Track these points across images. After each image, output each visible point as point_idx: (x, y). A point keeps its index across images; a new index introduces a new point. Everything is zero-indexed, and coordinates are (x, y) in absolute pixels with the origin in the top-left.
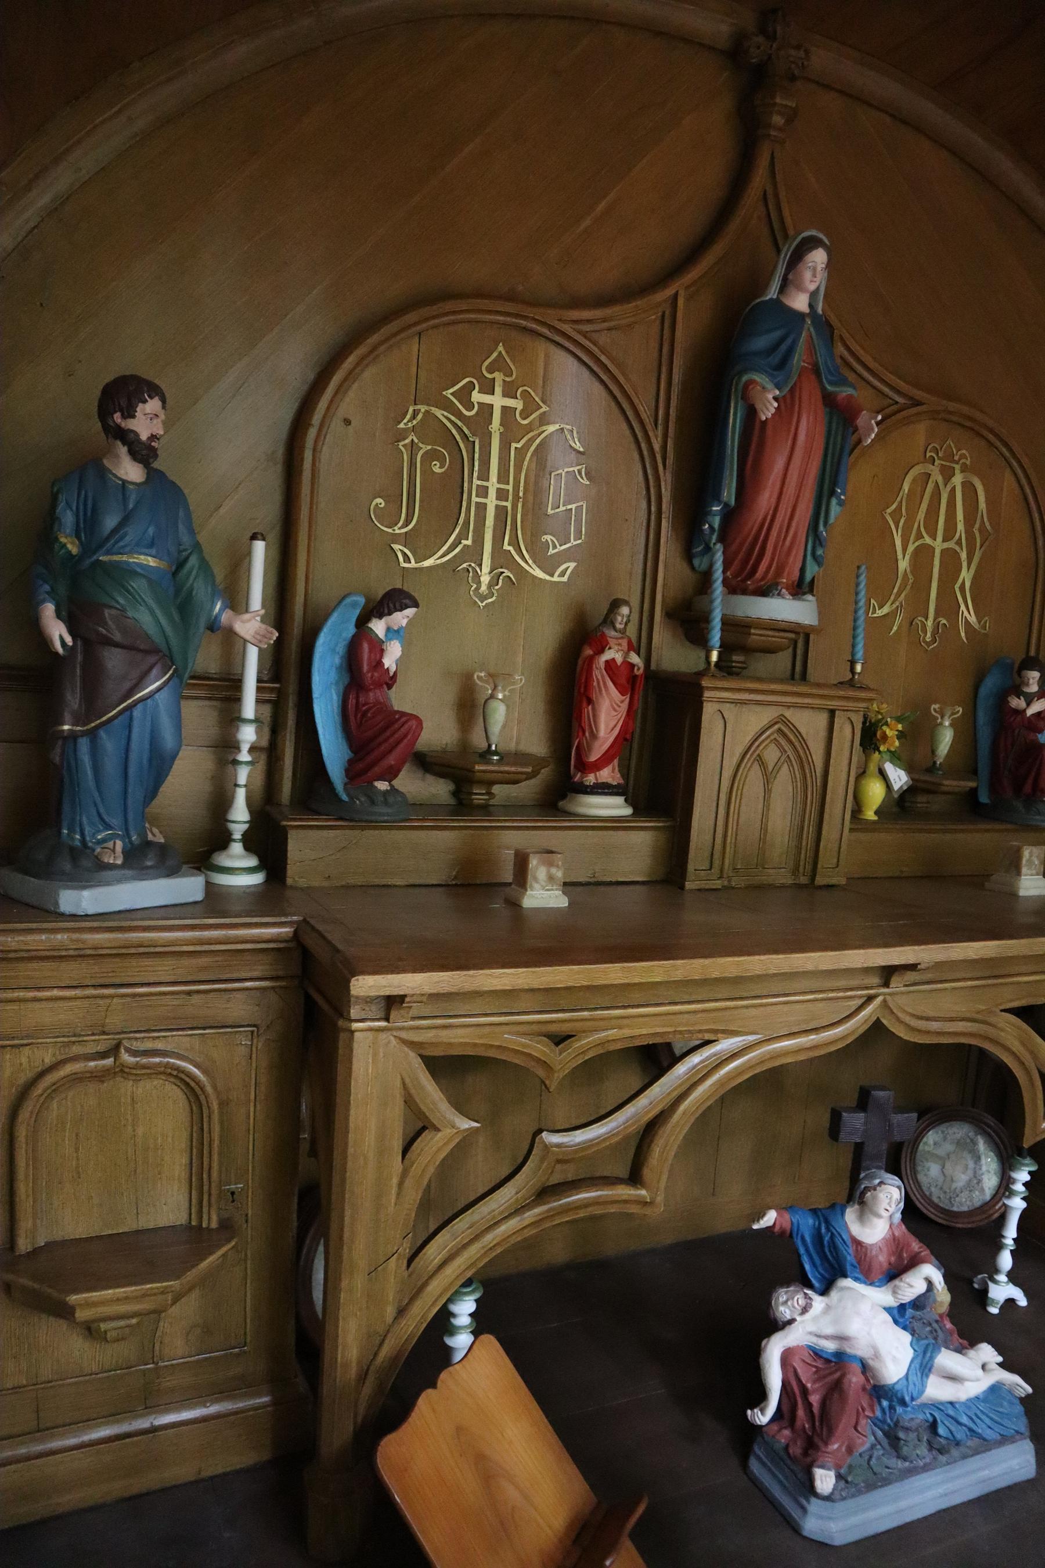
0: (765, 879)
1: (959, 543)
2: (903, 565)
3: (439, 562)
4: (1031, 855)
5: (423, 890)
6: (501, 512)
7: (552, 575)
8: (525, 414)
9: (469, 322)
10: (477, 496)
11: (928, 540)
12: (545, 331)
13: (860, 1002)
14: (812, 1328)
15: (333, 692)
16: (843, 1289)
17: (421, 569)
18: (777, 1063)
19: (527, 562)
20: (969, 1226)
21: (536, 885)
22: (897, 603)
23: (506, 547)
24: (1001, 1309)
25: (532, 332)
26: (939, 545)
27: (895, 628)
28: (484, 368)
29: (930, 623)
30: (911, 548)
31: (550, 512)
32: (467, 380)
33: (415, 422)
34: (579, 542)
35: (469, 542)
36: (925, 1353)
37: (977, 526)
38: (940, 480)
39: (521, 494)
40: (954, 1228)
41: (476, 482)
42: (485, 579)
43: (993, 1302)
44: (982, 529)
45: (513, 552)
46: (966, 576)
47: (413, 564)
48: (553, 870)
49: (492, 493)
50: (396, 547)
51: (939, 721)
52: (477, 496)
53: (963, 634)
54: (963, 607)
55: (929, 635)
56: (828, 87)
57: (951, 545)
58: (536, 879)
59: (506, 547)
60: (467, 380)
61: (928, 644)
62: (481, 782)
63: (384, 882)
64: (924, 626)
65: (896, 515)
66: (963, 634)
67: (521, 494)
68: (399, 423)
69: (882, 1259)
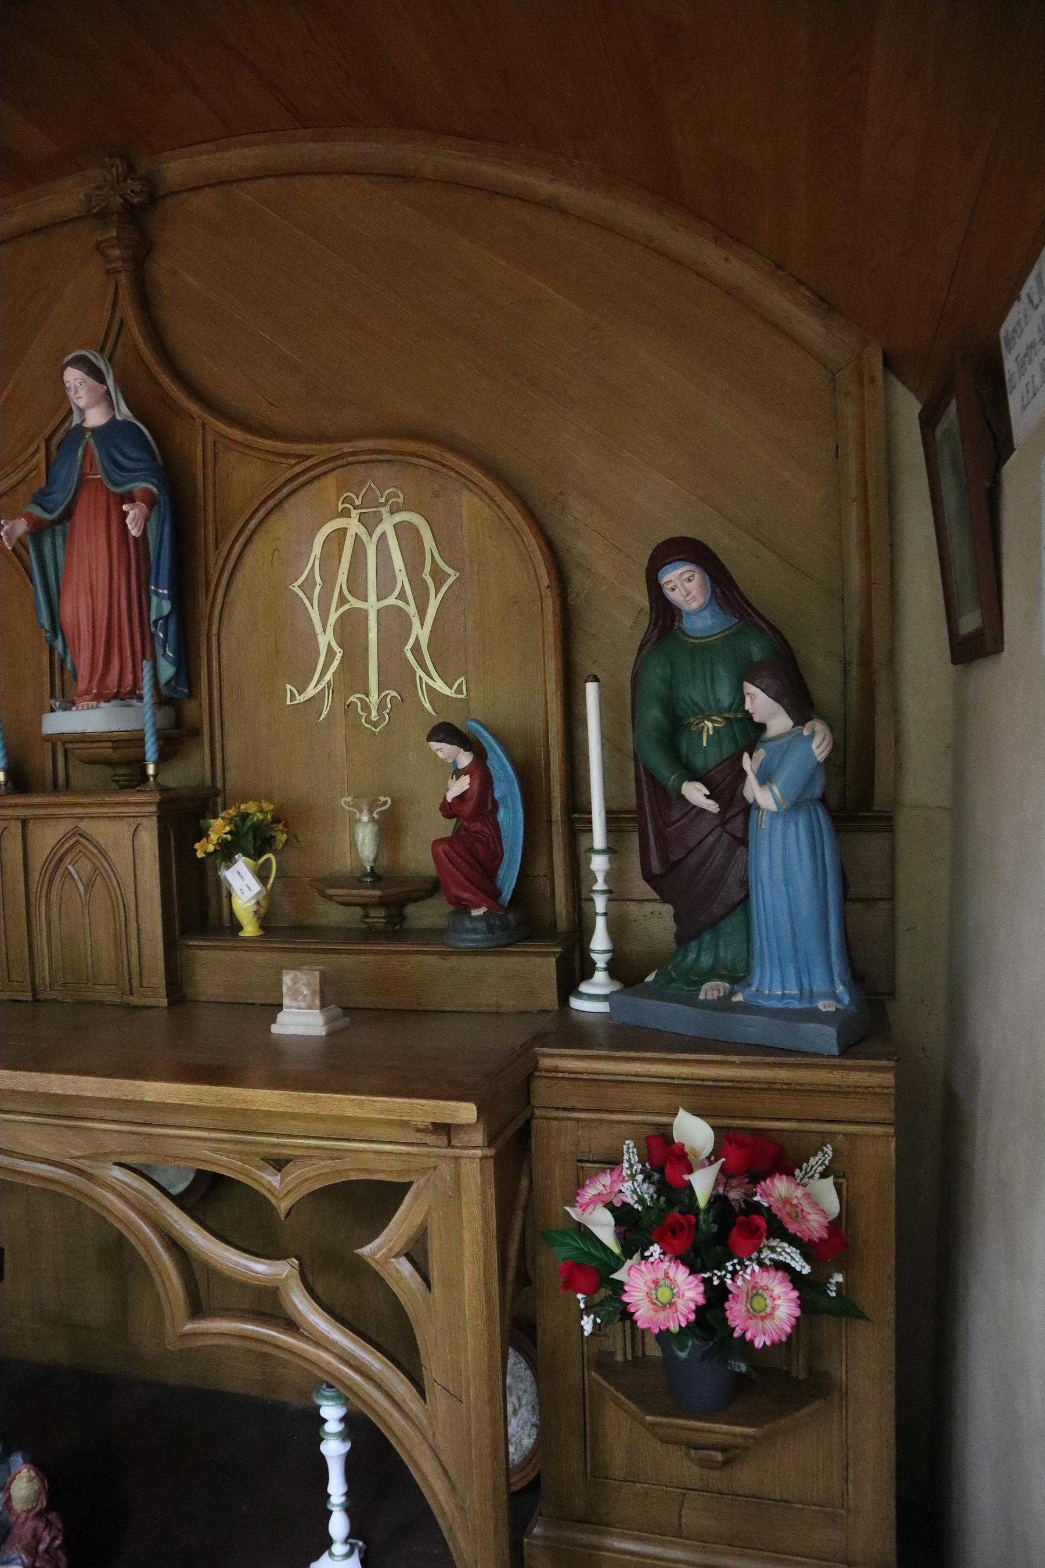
2: (326, 639)
4: (295, 981)
11: (356, 603)
22: (323, 683)
26: (372, 606)
27: (325, 712)
29: (374, 699)
46: (421, 632)
51: (358, 816)
53: (427, 706)
54: (420, 672)
55: (374, 713)
56: (197, 188)
57: (391, 600)
61: (375, 724)
64: (366, 708)
65: (307, 587)
66: (427, 706)
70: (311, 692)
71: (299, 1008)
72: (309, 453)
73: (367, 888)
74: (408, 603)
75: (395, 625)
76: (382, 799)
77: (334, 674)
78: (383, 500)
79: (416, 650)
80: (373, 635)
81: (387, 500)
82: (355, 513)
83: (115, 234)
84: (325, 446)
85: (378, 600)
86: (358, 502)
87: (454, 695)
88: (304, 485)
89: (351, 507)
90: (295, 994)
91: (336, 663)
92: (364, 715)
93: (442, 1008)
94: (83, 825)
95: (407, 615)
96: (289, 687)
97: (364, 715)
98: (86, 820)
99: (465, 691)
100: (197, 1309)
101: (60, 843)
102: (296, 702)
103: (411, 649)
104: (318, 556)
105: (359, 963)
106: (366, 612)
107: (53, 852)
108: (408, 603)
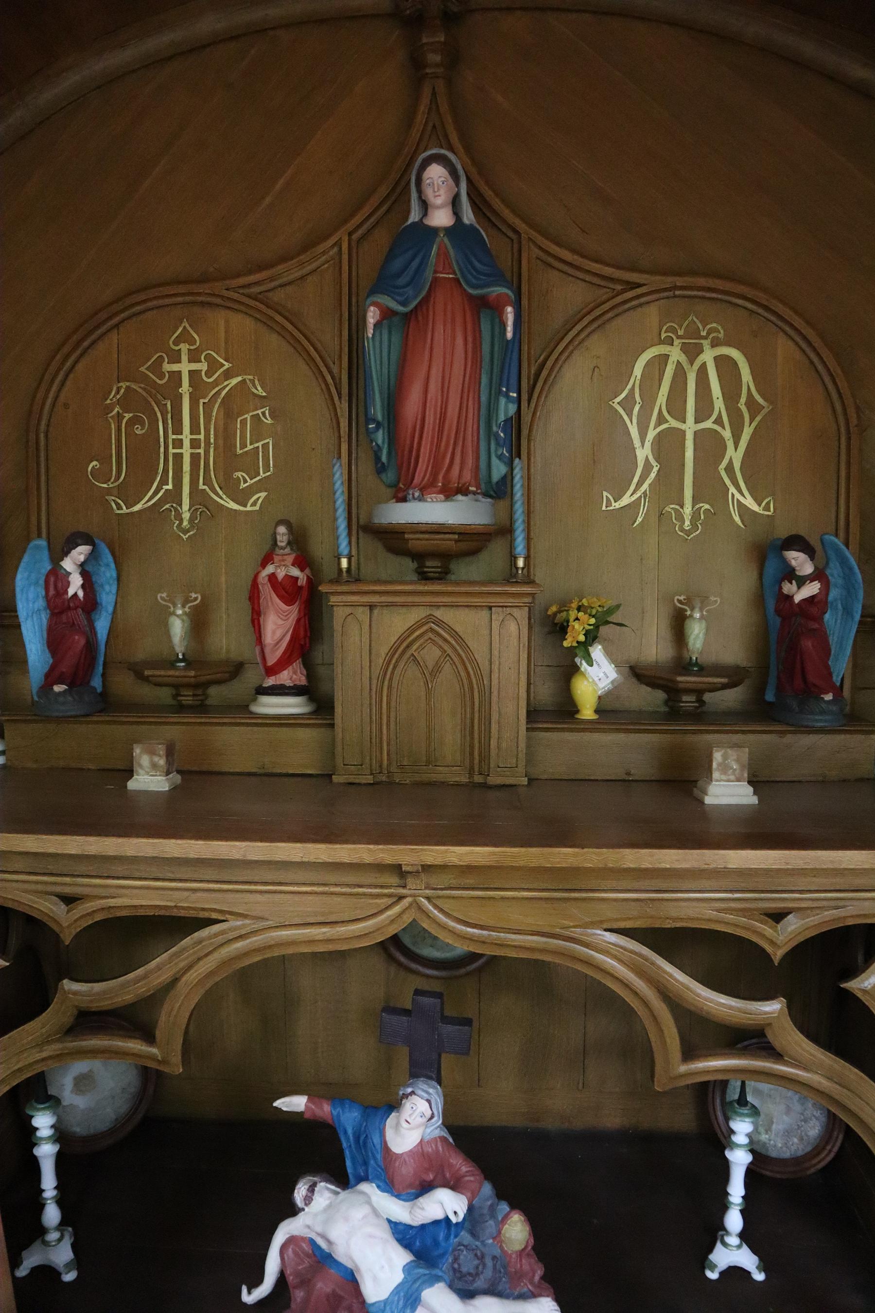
0: (434, 777)
1: (719, 421)
2: (643, 453)
3: (146, 506)
4: (725, 757)
5: (293, 780)
6: (195, 458)
7: (245, 506)
8: (209, 374)
9: (158, 307)
10: (173, 448)
11: (674, 423)
12: (219, 301)
13: (390, 901)
14: (309, 1223)
15: (43, 616)
16: (362, 1193)
17: (132, 513)
18: (276, 953)
19: (221, 498)
20: (778, 1176)
21: (140, 771)
22: (638, 494)
23: (202, 486)
24: (722, 1274)
25: (209, 304)
26: (690, 427)
27: (639, 519)
28: (171, 343)
29: (688, 510)
30: (651, 434)
31: (239, 452)
32: (158, 355)
33: (118, 397)
34: (269, 473)
35: (170, 487)
36: (415, 1281)
37: (743, 400)
38: (683, 359)
39: (212, 441)
40: (762, 1176)
41: (172, 437)
42: (186, 516)
43: (713, 1267)
44: (751, 403)
45: (208, 490)
46: (735, 455)
47: (125, 510)
48: (156, 759)
49: (187, 443)
50: (110, 498)
51: (688, 613)
52: (173, 448)
54: (732, 490)
55: (687, 523)
57: (708, 424)
58: (141, 766)
59: (202, 486)
60: (158, 355)
61: (688, 533)
62: (688, 691)
63: (79, 766)
64: (680, 518)
66: (737, 519)
67: (212, 441)
68: (106, 399)
69: (406, 1171)
70: (626, 500)
71: (728, 781)
72: (642, 281)
73: (695, 675)
74: (724, 428)
75: (710, 447)
76: (194, 595)
77: (650, 485)
78: (704, 333)
79: (730, 469)
80: (689, 454)
81: (708, 334)
82: (677, 342)
83: (442, 39)
84: (658, 278)
85: (696, 422)
86: (680, 333)
87: (761, 512)
88: (129, 318)
89: (674, 338)
90: (725, 768)
91: (653, 475)
92: (678, 524)
93: (772, 779)
94: (438, 613)
95: (722, 439)
96: (605, 494)
97: (678, 524)
98: (442, 609)
99: (772, 509)
100: (689, 1053)
101: (411, 630)
102: (611, 508)
103: (725, 469)
104: (639, 377)
105: (764, 739)
106: (684, 432)
107: (402, 639)
108: (724, 428)
